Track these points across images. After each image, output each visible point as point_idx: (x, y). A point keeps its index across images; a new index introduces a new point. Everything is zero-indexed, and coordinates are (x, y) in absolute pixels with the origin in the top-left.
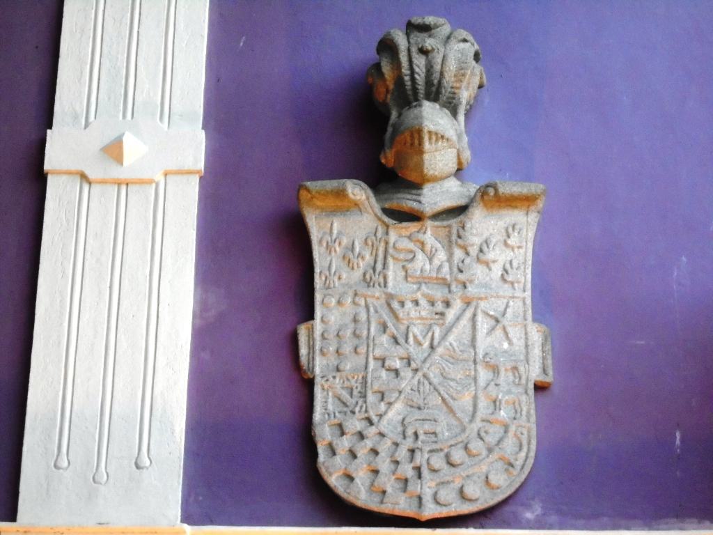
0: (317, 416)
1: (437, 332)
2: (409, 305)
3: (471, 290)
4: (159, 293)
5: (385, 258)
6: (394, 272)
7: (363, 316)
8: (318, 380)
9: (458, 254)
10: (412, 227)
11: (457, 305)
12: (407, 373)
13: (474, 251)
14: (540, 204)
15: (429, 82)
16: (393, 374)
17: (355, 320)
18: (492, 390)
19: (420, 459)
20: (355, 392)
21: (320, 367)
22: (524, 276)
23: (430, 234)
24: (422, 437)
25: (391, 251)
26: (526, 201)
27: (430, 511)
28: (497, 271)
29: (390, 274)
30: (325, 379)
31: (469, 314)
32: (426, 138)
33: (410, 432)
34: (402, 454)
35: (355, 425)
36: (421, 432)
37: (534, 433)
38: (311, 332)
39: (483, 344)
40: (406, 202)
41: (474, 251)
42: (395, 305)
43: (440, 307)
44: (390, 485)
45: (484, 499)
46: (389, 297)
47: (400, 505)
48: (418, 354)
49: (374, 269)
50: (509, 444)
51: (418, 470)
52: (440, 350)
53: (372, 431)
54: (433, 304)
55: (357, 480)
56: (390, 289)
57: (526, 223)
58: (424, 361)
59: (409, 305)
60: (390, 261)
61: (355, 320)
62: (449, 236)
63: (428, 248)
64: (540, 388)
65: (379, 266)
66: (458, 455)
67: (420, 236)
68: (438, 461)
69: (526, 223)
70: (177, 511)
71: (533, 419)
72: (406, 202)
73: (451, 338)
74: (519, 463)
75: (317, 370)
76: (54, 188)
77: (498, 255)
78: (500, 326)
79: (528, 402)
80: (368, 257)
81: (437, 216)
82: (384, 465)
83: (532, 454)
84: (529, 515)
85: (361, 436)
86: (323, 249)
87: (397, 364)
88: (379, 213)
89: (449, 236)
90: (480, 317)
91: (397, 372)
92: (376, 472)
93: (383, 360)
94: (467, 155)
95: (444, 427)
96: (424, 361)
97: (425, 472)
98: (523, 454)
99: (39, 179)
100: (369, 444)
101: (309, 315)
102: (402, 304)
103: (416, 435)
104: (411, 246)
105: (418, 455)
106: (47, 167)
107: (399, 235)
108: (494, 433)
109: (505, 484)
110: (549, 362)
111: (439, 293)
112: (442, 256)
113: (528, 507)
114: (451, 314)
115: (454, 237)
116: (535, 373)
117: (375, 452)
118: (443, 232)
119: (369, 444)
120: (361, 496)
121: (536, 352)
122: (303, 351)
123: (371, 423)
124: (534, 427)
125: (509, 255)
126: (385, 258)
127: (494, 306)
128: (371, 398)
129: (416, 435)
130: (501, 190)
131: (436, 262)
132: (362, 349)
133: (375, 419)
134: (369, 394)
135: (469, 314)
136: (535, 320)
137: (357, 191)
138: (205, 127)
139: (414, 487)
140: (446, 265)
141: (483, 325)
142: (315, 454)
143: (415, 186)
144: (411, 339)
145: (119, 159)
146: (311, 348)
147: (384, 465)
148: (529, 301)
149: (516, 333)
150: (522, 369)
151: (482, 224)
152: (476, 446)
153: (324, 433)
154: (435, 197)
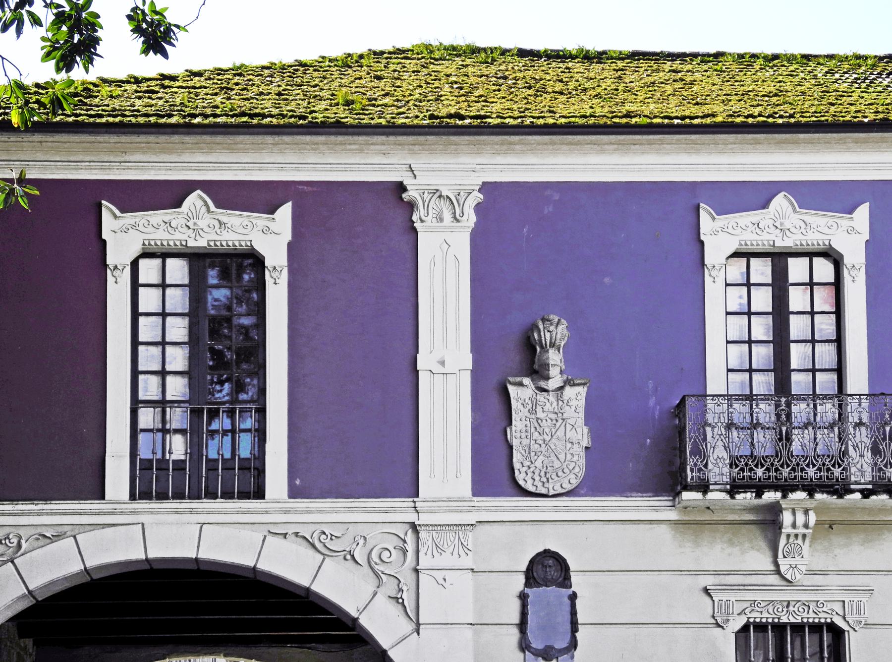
0: (515, 460)
1: (554, 431)
2: (544, 421)
3: (565, 416)
4: (603, 624)
5: (536, 405)
6: (539, 409)
7: (529, 425)
8: (514, 447)
9: (561, 403)
10: (545, 394)
11: (560, 421)
12: (543, 446)
13: (566, 402)
14: (588, 385)
15: (551, 342)
16: (539, 446)
17: (526, 426)
18: (571, 451)
19: (548, 475)
20: (527, 452)
21: (515, 443)
22: (582, 410)
23: (552, 397)
24: (549, 468)
25: (538, 402)
26: (584, 384)
27: (552, 492)
28: (573, 408)
29: (537, 410)
30: (438, 194)
31: (564, 422)
32: (551, 366)
33: (545, 466)
34: (542, 474)
35: (527, 463)
36: (548, 466)
37: (584, 465)
38: (511, 430)
39: (569, 435)
40: (542, 384)
41: (566, 402)
42: (540, 421)
43: (554, 422)
44: (539, 485)
45: (568, 487)
46: (538, 419)
47: (543, 491)
48: (547, 438)
49: (532, 408)
50: (577, 470)
51: (548, 479)
52: (554, 437)
53: (532, 465)
54: (552, 420)
55: (528, 482)
56: (538, 416)
57: (583, 390)
58: (549, 441)
59: (544, 421)
60: (538, 406)
61: (526, 426)
62: (558, 396)
63: (550, 401)
64: (586, 448)
65: (534, 408)
66: (560, 474)
67: (548, 397)
68: (554, 476)
69: (583, 390)
70: (470, 493)
71: (584, 460)
72: (542, 384)
73: (558, 433)
74: (579, 475)
75: (514, 444)
76: (423, 377)
77: (573, 403)
78: (574, 429)
79: (583, 454)
80: (531, 405)
81: (552, 391)
82: (537, 478)
83: (584, 472)
84: (582, 492)
85: (529, 468)
86: (515, 400)
87: (541, 442)
88: (534, 389)
89: (558, 396)
90: (567, 425)
91: (540, 445)
92: (534, 480)
93: (536, 440)
94: (563, 367)
95: (557, 464)
96: (549, 441)
97: (550, 479)
98: (581, 472)
99: (416, 372)
100: (532, 470)
101: (510, 424)
102: (542, 421)
103: (547, 467)
104: (545, 400)
105: (548, 474)
106: (418, 369)
107: (541, 397)
108: (572, 465)
109: (575, 482)
110: (590, 440)
111: (553, 416)
112: (555, 404)
113: (582, 489)
114: (558, 424)
115: (559, 397)
116: (585, 443)
117: (533, 472)
118: (556, 396)
119: (532, 470)
120: (532, 489)
121: (586, 436)
122: (509, 436)
123: (532, 463)
124: (584, 463)
125: (577, 402)
126: (536, 405)
127: (572, 422)
128: (532, 454)
129: (547, 467)
130: (575, 382)
131: (553, 406)
132: (529, 437)
133: (533, 461)
134: (532, 453)
135: (564, 422)
136: (585, 425)
137: (527, 381)
138: (471, 352)
139: (546, 485)
140: (556, 407)
141: (569, 427)
142: (514, 473)
143: (547, 378)
144: (545, 434)
145: (444, 366)
146: (512, 436)
147: (537, 478)
148: (583, 419)
149: (579, 430)
150: (581, 443)
151: (569, 392)
152: (566, 470)
153: (517, 466)
154: (554, 382)
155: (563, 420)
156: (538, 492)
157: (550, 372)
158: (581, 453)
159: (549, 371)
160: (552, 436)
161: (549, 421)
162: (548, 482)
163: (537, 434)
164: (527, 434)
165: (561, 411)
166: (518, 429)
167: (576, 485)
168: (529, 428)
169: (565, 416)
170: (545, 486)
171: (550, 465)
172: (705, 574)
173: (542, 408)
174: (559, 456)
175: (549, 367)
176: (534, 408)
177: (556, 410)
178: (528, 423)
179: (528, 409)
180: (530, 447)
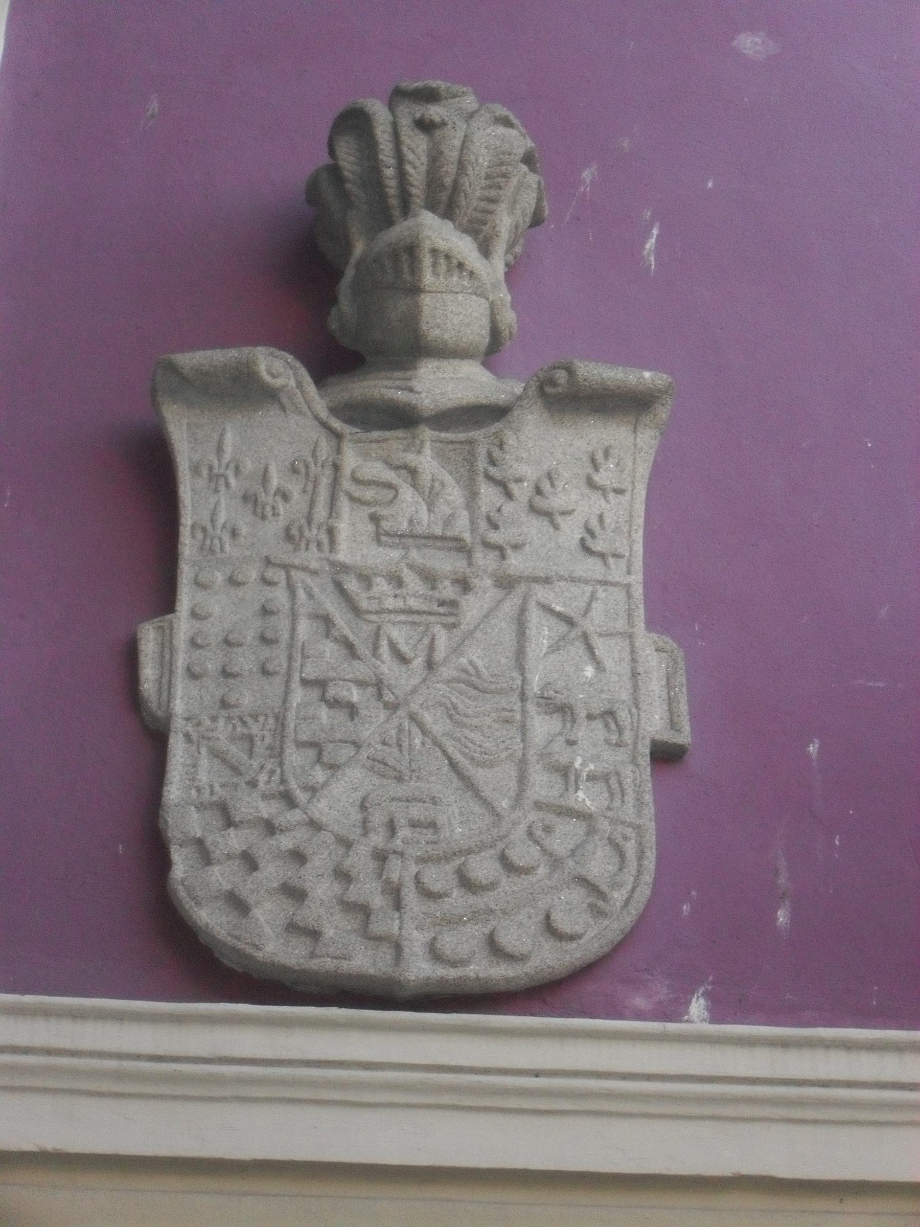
8: (178, 724)
10: (395, 440)
13: (522, 492)
15: (433, 182)
19: (395, 870)
20: (259, 748)
24: (404, 832)
25: (346, 484)
32: (427, 261)
37: (651, 838)
38: (167, 646)
42: (352, 585)
43: (448, 591)
56: (342, 556)
59: (381, 585)
60: (344, 504)
62: (471, 460)
65: (321, 512)
67: (410, 458)
71: (650, 811)
74: (618, 896)
75: (179, 707)
86: (202, 483)
112: (455, 494)
115: (482, 464)
121: (655, 687)
122: (148, 672)
123: (289, 800)
124: (650, 827)
131: (444, 509)
135: (510, 606)
136: (651, 625)
144: (384, 650)
146: (166, 665)
148: (638, 591)
155: (506, 583)
156: (325, 964)
157: (426, 300)
158: (628, 771)
159: (415, 290)
160: (430, 665)
161: (412, 582)
162: (398, 905)
163: (329, 650)
164: (265, 652)
165: (494, 537)
166: (214, 631)
167: (628, 920)
168: (282, 625)
169: (516, 563)
170: (377, 927)
171: (416, 811)
172: (549, 1113)
173: (375, 519)
174: (480, 775)
175: (415, 269)
176: (321, 512)
177: (462, 527)
178: (280, 596)
179: (281, 523)
180: (281, 721)
